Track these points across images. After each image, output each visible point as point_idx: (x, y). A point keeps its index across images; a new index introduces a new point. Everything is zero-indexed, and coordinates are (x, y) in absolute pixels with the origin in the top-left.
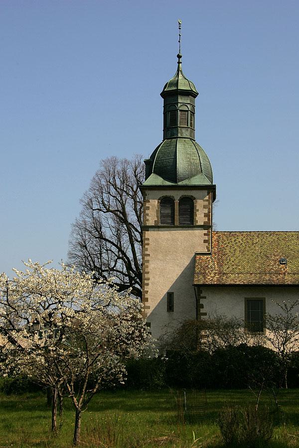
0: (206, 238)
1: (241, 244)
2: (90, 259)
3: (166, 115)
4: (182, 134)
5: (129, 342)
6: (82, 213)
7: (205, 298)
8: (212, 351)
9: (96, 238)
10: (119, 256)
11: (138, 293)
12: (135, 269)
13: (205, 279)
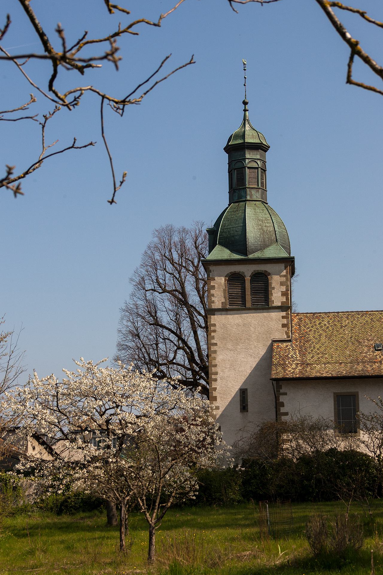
0: (285, 321)
1: (328, 328)
2: (143, 350)
3: (232, 175)
4: (251, 196)
5: (200, 451)
6: (133, 295)
7: (285, 394)
8: (296, 458)
9: (151, 324)
10: (179, 345)
11: (206, 392)
12: (199, 362)
13: (285, 372)
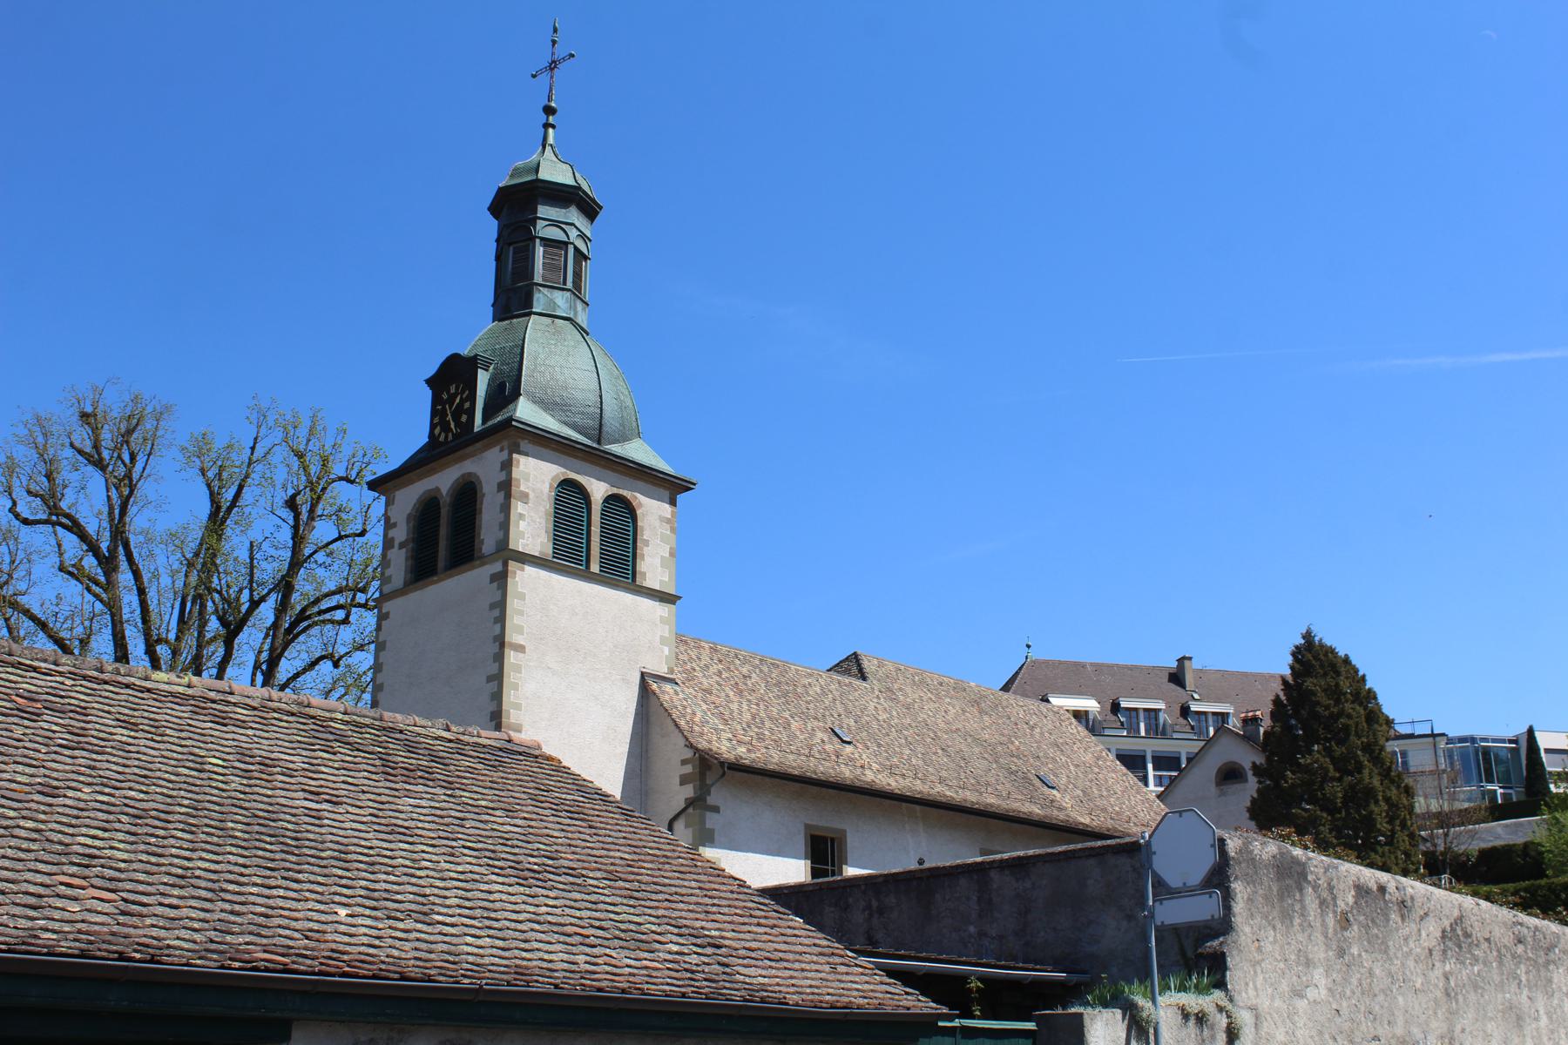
7: (716, 809)
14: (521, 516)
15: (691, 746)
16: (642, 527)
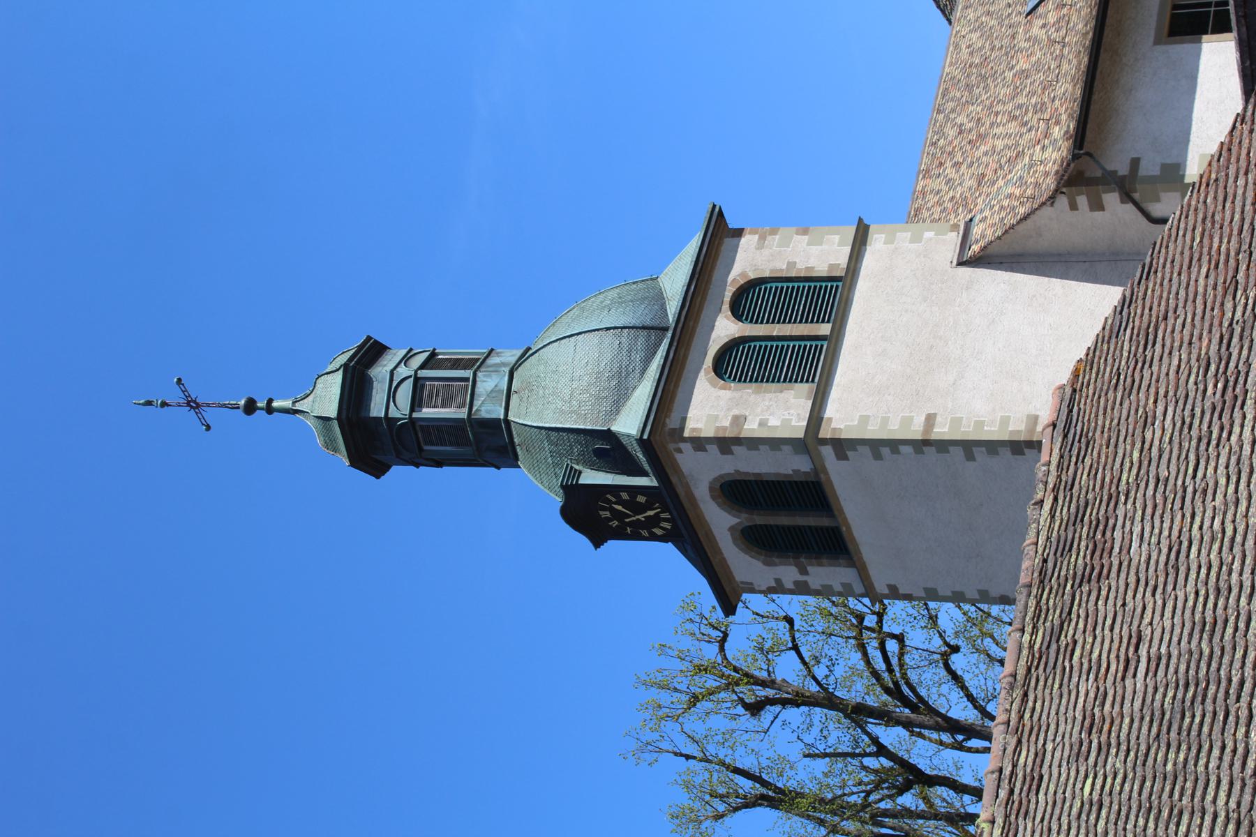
14: (763, 424)
15: (1052, 198)
16: (772, 271)
